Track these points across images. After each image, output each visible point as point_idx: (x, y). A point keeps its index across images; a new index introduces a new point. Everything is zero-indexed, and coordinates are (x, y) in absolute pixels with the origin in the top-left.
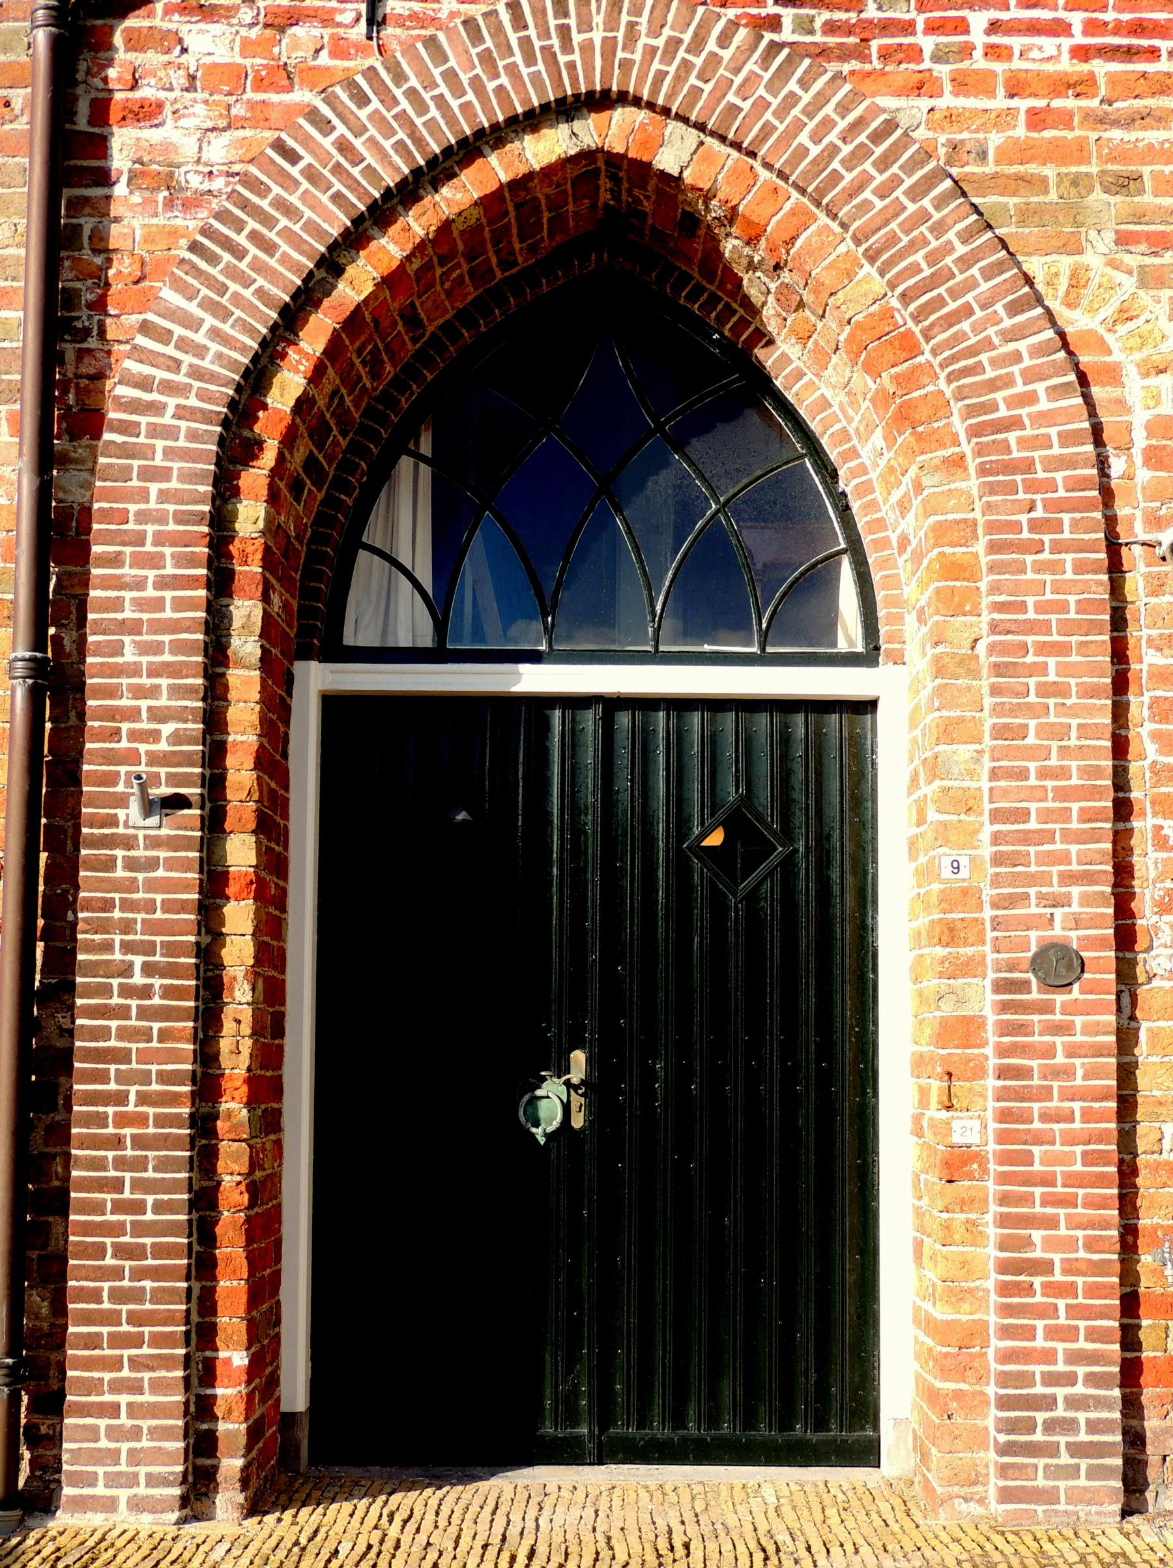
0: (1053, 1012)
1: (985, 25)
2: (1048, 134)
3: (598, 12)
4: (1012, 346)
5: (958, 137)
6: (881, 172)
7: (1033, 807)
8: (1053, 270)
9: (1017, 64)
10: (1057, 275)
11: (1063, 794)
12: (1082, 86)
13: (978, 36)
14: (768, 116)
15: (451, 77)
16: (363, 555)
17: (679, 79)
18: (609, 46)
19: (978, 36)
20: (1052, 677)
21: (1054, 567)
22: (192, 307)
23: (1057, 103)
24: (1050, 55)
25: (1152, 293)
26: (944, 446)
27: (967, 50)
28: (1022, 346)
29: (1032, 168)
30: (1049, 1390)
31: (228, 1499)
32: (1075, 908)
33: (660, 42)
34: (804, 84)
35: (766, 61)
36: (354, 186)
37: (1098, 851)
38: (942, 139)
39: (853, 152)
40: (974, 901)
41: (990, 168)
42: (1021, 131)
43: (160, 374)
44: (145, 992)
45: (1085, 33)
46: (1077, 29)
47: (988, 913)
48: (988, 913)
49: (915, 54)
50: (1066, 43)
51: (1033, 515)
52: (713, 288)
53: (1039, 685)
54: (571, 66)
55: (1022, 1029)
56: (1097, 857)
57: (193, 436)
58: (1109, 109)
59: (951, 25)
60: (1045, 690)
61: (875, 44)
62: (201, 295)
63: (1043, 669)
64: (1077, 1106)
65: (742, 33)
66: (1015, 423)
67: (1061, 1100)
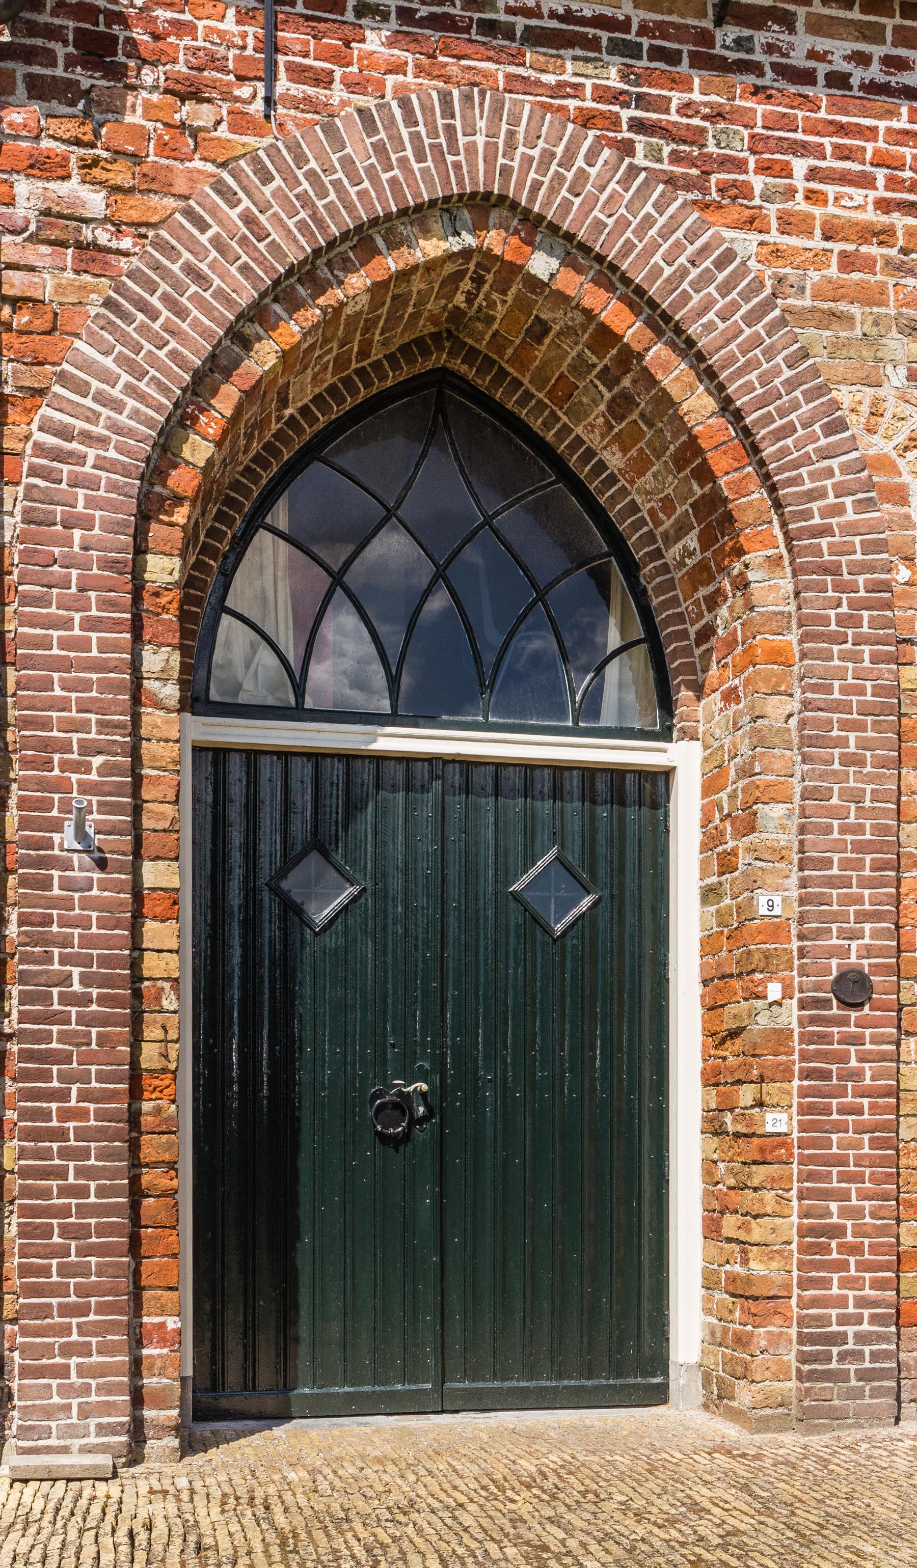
0: (849, 1025)
1: (804, 171)
2: (856, 276)
3: (481, 117)
4: (826, 463)
5: (783, 271)
6: (723, 297)
7: (836, 857)
8: (857, 398)
9: (831, 209)
10: (860, 403)
11: (859, 847)
12: (884, 236)
13: (799, 182)
14: (629, 234)
15: (347, 162)
16: (226, 620)
17: (553, 190)
18: (491, 148)
19: (799, 182)
20: (852, 749)
21: (856, 658)
22: (108, 362)
23: (864, 249)
24: (857, 205)
25: (175, 605)
26: (766, 547)
27: (790, 192)
28: (835, 463)
29: (842, 306)
30: (842, 1328)
31: (161, 1446)
32: (867, 941)
33: (536, 153)
34: (660, 207)
35: (626, 183)
36: (261, 261)
37: (886, 894)
38: (769, 272)
39: (700, 275)
40: (785, 934)
41: (808, 303)
42: (833, 271)
43: (80, 425)
44: (85, 1000)
45: (887, 188)
46: (881, 182)
47: (795, 944)
48: (795, 944)
49: (745, 191)
50: (872, 195)
51: (839, 610)
52: (541, 395)
53: (842, 755)
54: (457, 166)
55: (824, 1038)
56: (885, 899)
57: (113, 487)
58: (905, 258)
59: (777, 168)
60: (847, 760)
61: (714, 178)
62: (116, 351)
63: (844, 742)
64: (866, 1101)
65: (606, 153)
66: (826, 531)
67: (854, 1096)
